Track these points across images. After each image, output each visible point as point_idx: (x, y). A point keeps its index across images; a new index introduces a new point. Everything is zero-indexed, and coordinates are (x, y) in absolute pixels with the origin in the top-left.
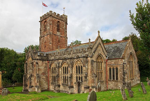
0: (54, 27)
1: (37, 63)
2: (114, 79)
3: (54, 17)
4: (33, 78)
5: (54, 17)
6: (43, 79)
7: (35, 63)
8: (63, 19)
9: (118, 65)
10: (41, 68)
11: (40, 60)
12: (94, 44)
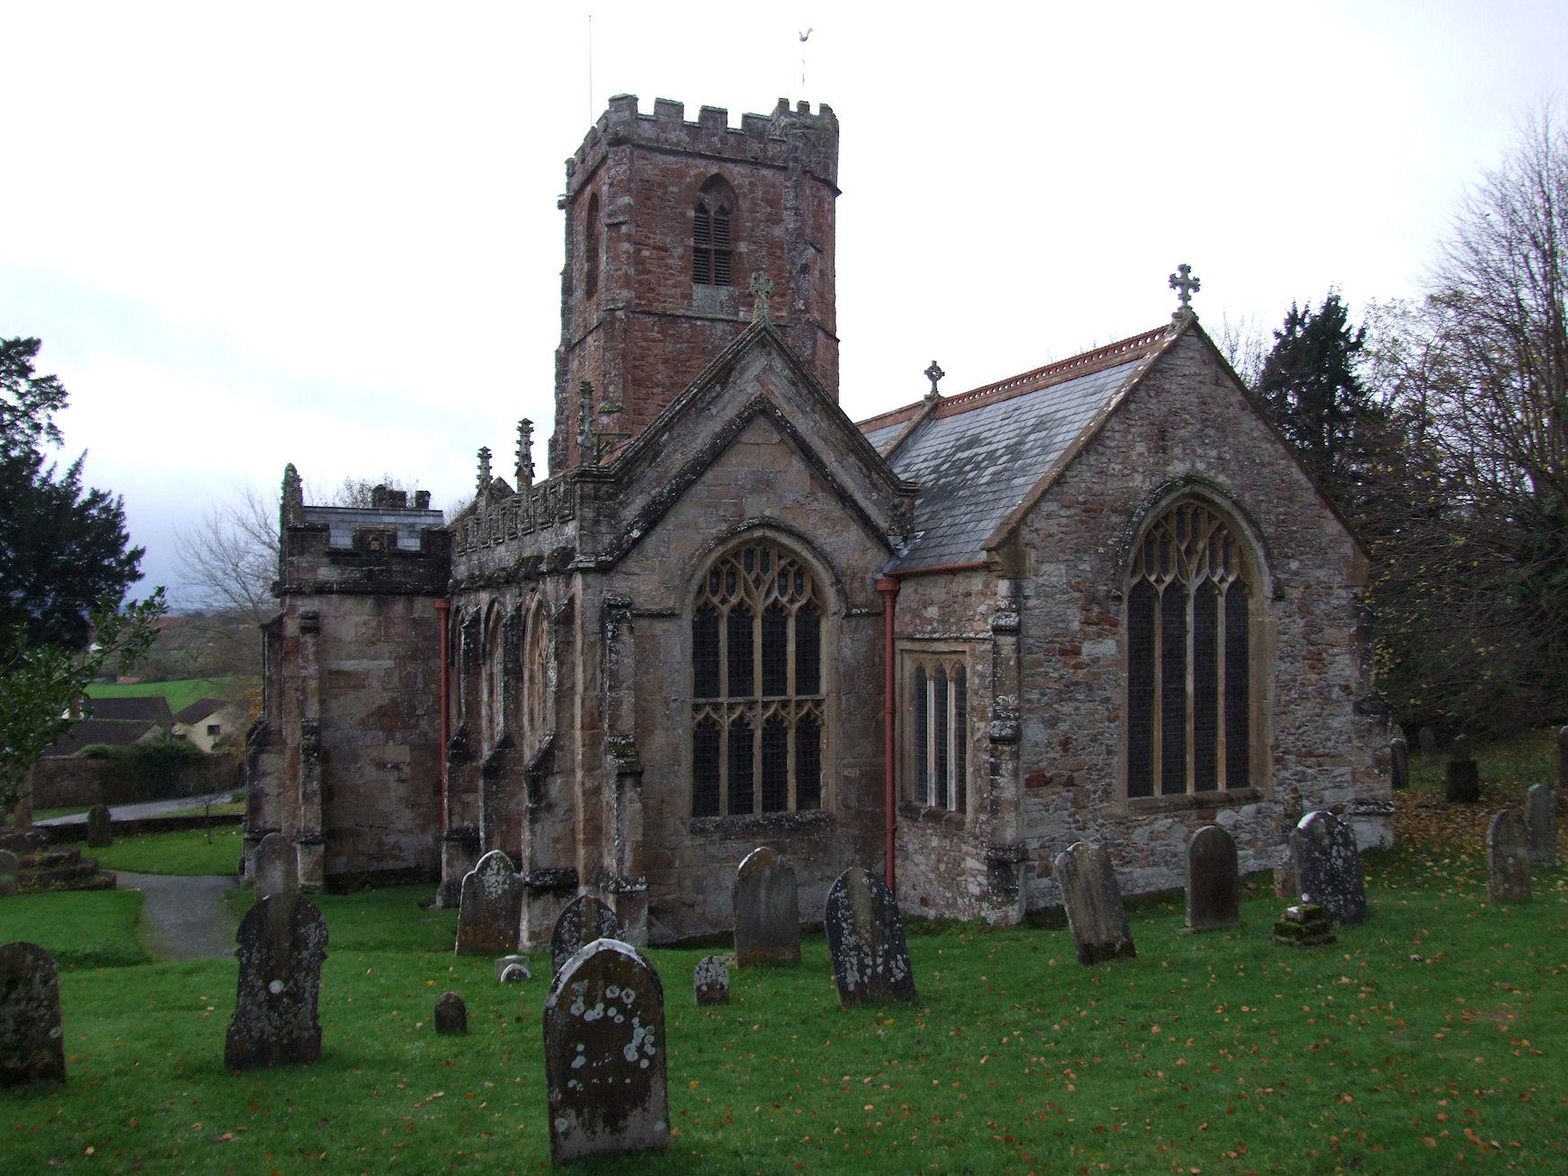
0: (657, 239)
1: (312, 625)
2: (774, 799)
3: (652, 149)
4: (272, 762)
5: (652, 149)
6: (381, 765)
7: (292, 627)
8: (772, 150)
9: (966, 647)
10: (365, 664)
11: (348, 591)
12: (668, 426)
